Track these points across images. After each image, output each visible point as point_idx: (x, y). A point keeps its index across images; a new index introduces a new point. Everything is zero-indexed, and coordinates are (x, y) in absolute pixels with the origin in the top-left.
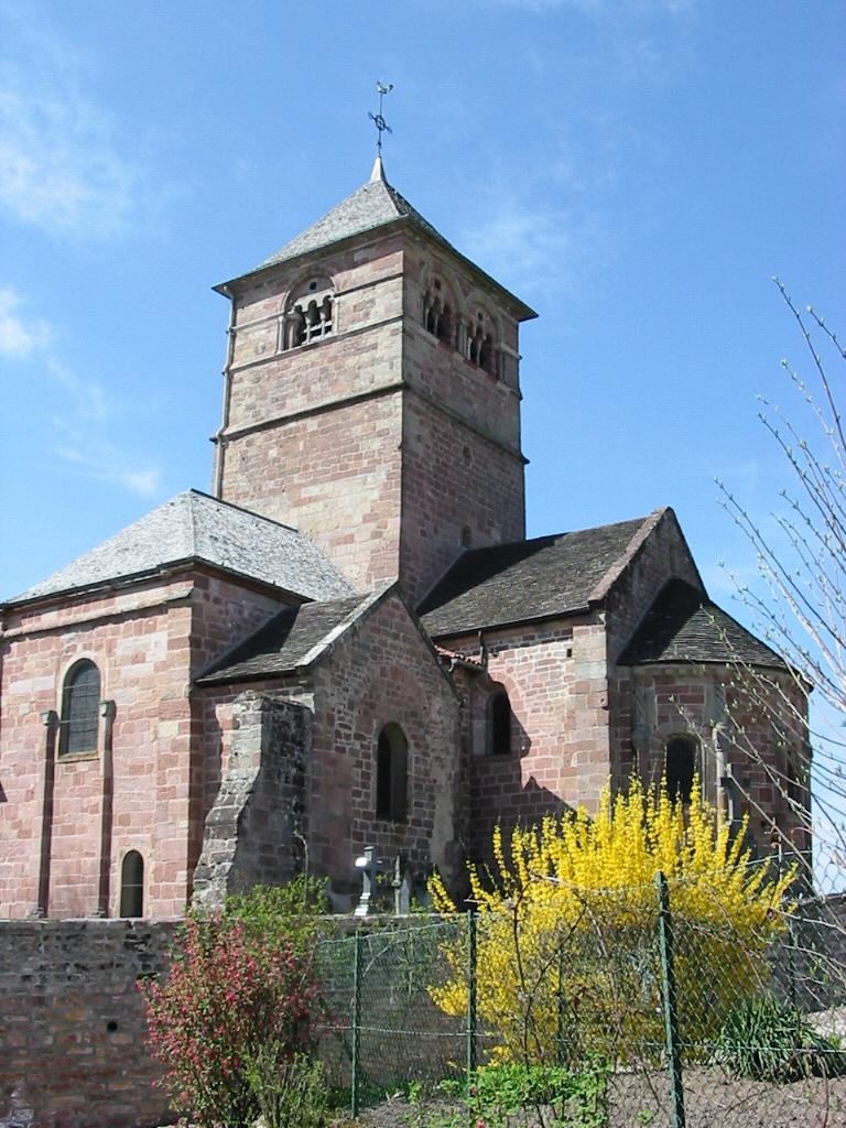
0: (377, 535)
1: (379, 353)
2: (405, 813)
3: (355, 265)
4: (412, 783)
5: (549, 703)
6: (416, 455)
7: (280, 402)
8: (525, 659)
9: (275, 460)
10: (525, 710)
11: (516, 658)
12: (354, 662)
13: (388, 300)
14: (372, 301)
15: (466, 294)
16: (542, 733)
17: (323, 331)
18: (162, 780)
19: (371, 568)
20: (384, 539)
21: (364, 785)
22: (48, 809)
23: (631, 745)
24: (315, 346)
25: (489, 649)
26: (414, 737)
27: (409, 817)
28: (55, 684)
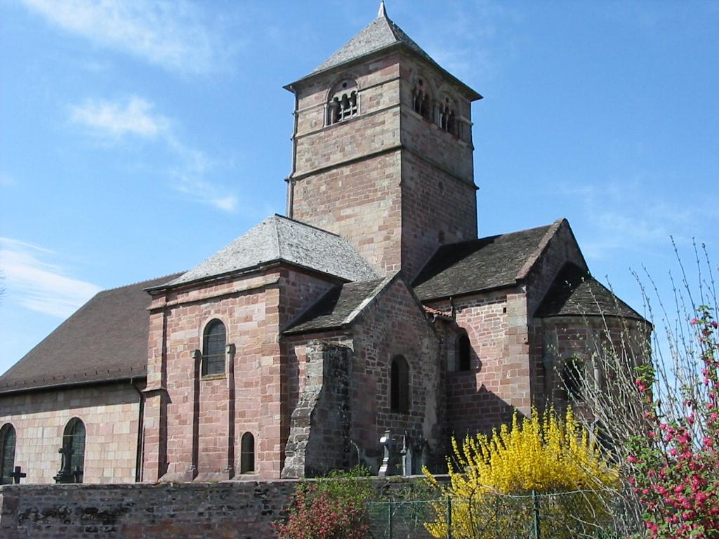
0: (387, 238)
1: (386, 127)
2: (408, 408)
3: (370, 72)
4: (411, 390)
6: (410, 189)
8: (478, 314)
11: (473, 313)
13: (391, 94)
14: (381, 95)
15: (438, 87)
16: (489, 358)
18: (264, 391)
19: (384, 258)
20: (392, 241)
22: (197, 408)
25: (456, 308)
28: (199, 334)
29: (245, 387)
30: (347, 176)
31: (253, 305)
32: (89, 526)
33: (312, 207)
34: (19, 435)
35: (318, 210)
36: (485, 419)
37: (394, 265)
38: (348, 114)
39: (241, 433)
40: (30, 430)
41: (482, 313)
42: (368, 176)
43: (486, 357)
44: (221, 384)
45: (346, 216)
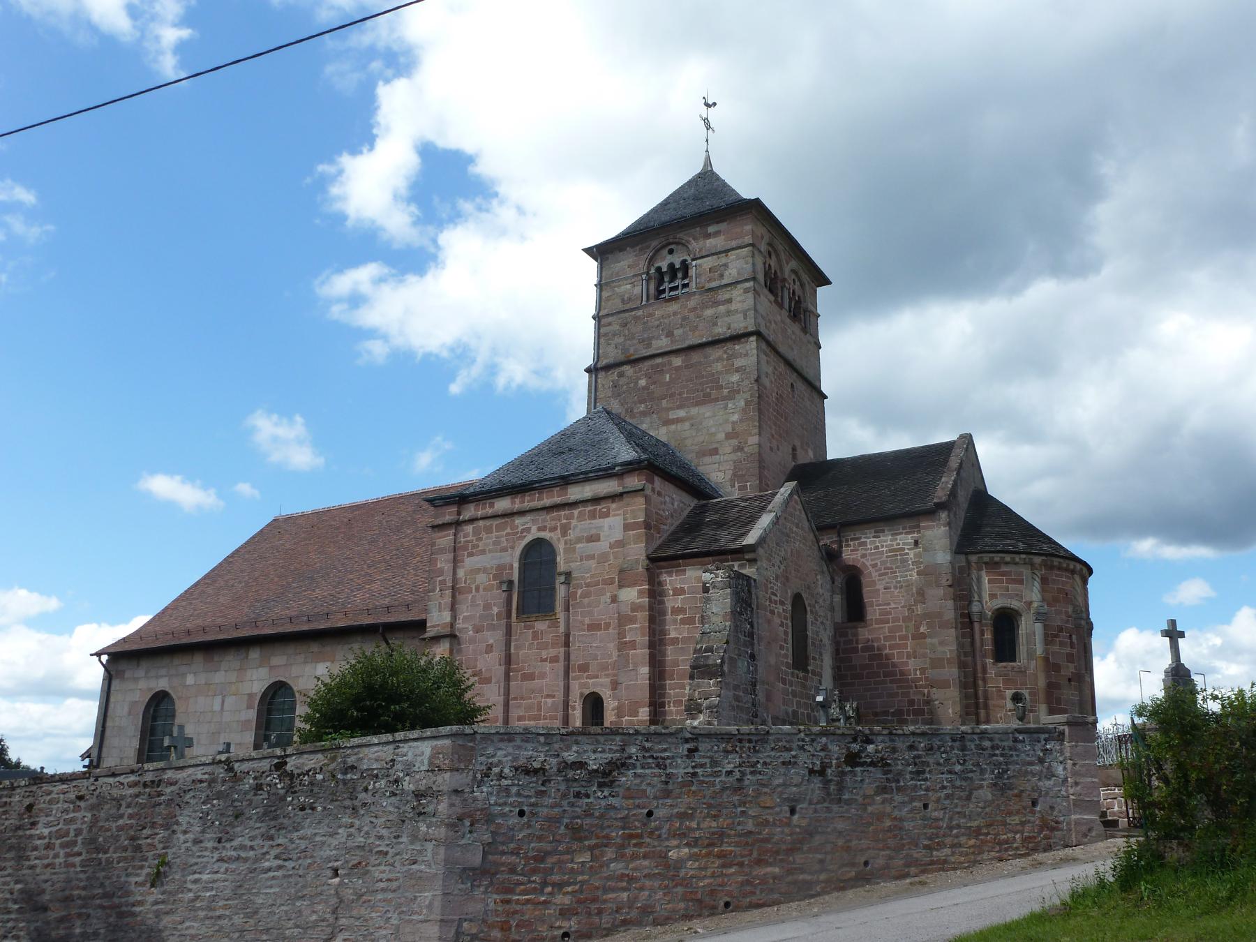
0: (740, 449)
1: (733, 307)
2: (807, 665)
3: (708, 236)
4: (810, 641)
5: (900, 582)
6: (765, 388)
7: (647, 342)
8: (877, 548)
9: (644, 388)
10: (877, 587)
12: (777, 544)
13: (738, 265)
14: (726, 265)
15: (787, 264)
17: (680, 287)
18: (621, 635)
19: (734, 475)
20: (745, 452)
21: (786, 641)
22: (508, 660)
23: (969, 616)
24: (676, 298)
25: (844, 539)
26: (810, 605)
27: (810, 668)
29: (588, 630)
30: (678, 368)
31: (602, 520)
32: (578, 789)
33: (626, 406)
34: (180, 707)
35: (635, 411)
36: (889, 685)
37: (748, 484)
38: (676, 288)
39: (582, 694)
40: (201, 700)
41: (882, 546)
42: (709, 369)
43: (889, 604)
44: (549, 627)
45: (677, 418)
